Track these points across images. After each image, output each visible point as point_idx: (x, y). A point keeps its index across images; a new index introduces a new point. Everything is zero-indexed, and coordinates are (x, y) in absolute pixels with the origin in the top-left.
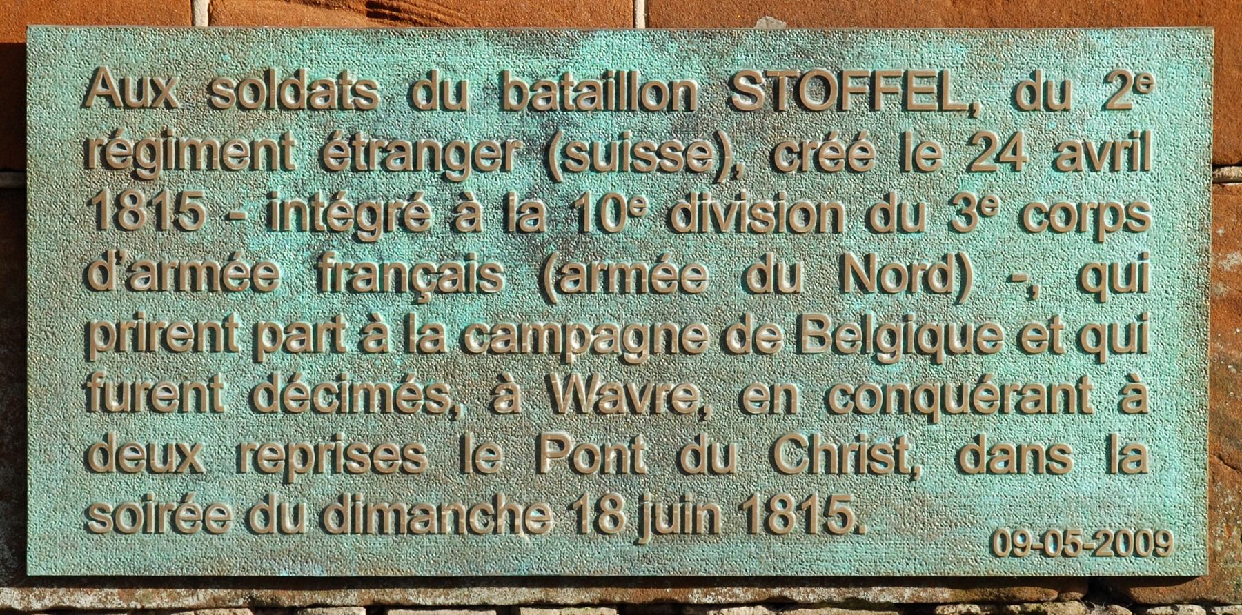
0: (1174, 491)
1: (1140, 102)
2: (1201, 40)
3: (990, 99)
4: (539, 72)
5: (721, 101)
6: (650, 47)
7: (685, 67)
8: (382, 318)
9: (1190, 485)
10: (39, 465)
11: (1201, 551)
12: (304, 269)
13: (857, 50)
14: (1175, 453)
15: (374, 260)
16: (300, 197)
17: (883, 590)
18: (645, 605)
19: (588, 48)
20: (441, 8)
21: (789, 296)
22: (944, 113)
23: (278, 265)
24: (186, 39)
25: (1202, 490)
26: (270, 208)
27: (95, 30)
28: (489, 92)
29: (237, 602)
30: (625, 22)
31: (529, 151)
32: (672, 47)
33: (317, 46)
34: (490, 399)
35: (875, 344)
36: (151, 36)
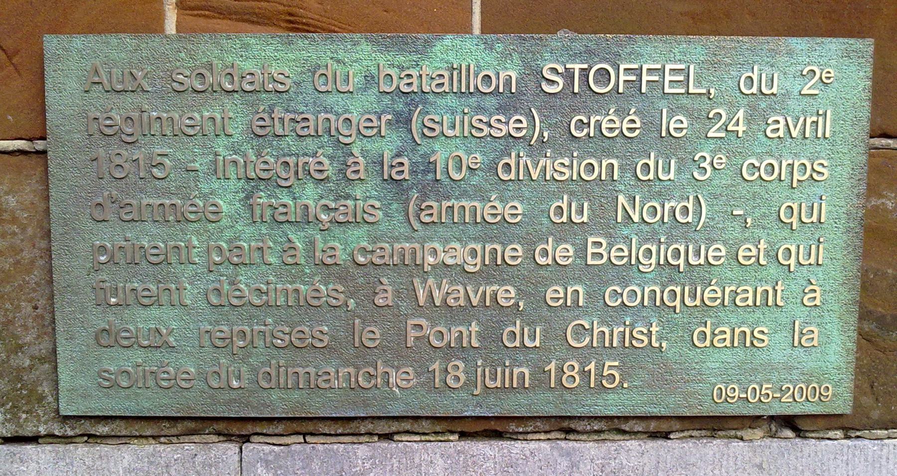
0: (833, 358)
1: (823, 89)
2: (866, 46)
3: (721, 86)
4: (404, 64)
5: (532, 85)
6: (483, 46)
7: (508, 61)
8: (296, 241)
9: (844, 353)
10: (64, 342)
11: (848, 396)
12: (240, 206)
13: (629, 50)
14: (835, 333)
15: (289, 199)
16: (236, 155)
17: (636, 424)
18: (482, 13)
19: (438, 47)
20: (336, 23)
21: (578, 225)
22: (689, 96)
23: (221, 203)
24: (155, 41)
25: (851, 358)
26: (215, 162)
27: (91, 37)
28: (369, 79)
29: (205, 431)
30: (464, 28)
31: (397, 122)
32: (499, 47)
33: (246, 46)
34: (43, 244)
35: (637, 258)
36: (129, 40)
